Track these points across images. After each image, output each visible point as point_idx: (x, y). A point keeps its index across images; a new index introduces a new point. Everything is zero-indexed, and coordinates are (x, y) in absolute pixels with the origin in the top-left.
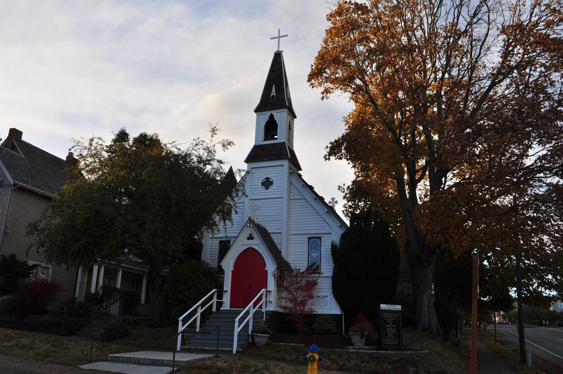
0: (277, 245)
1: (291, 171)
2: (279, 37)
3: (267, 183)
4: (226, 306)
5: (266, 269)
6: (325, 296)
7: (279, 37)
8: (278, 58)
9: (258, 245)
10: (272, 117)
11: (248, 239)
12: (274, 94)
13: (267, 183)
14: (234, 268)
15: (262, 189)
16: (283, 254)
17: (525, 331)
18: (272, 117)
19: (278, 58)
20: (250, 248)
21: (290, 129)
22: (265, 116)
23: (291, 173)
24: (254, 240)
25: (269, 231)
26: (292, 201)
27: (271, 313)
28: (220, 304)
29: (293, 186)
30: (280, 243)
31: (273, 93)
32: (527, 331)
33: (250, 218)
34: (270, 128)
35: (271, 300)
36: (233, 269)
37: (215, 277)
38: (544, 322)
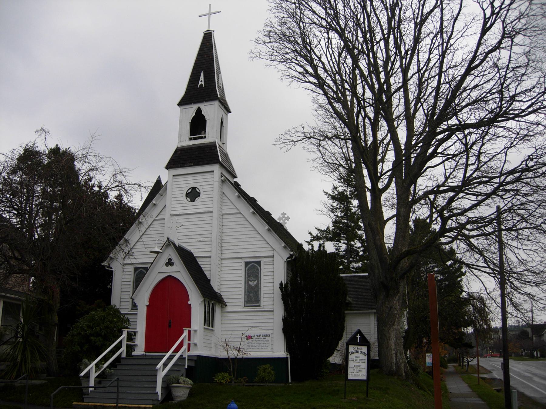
0: (205, 273)
1: (223, 178)
2: (210, 14)
3: (193, 194)
4: (140, 350)
5: (189, 303)
6: (267, 336)
7: (210, 14)
8: (208, 38)
9: (180, 272)
10: (199, 111)
11: (170, 260)
12: (203, 83)
13: (193, 194)
14: (150, 301)
15: (186, 201)
16: (242, 187)
17: (510, 363)
18: (199, 111)
19: (208, 38)
20: (170, 276)
21: (222, 123)
22: (191, 111)
23: (223, 182)
24: (174, 266)
25: (196, 255)
26: (225, 217)
27: (196, 359)
28: (130, 349)
29: (225, 198)
30: (208, 269)
31: (202, 81)
32: (515, 366)
33: (168, 239)
34: (198, 125)
35: (196, 342)
36: (148, 304)
37: (117, 323)
38: (535, 353)
